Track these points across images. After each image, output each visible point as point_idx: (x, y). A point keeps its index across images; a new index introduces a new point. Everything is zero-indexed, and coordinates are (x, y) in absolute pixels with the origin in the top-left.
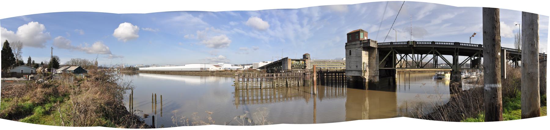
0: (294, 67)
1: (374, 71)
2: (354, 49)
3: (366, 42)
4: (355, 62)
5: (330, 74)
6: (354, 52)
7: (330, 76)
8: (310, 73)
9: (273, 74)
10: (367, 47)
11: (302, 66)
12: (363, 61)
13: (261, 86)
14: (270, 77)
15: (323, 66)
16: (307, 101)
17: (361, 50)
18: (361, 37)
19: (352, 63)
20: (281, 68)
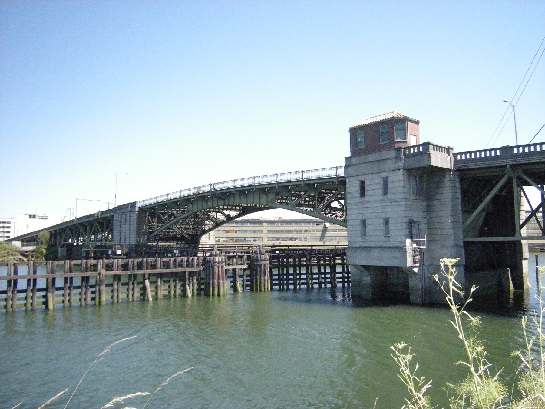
2: (374, 175)
3: (415, 154)
6: (377, 187)
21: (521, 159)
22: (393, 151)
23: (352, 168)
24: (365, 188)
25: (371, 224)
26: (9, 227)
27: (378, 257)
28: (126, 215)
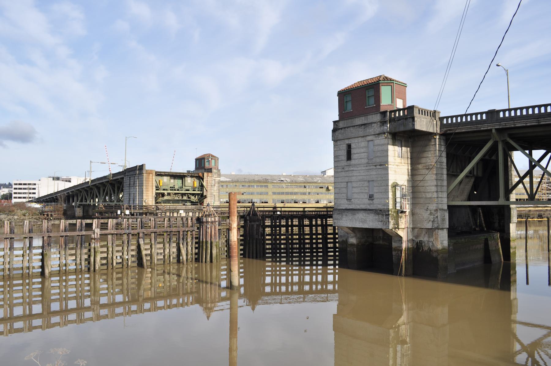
0: (166, 198)
2: (360, 139)
3: (400, 118)
4: (366, 184)
5: (283, 222)
6: (362, 150)
7: (283, 229)
8: (217, 219)
9: (89, 221)
10: (404, 132)
11: (193, 194)
12: (392, 178)
13: (42, 267)
14: (77, 233)
15: (261, 194)
16: (208, 310)
17: (386, 141)
18: (385, 100)
19: (354, 185)
20: (119, 200)
21: (506, 123)
22: (379, 115)
23: (340, 131)
24: (352, 151)
26: (34, 189)
27: (362, 219)
28: (130, 177)
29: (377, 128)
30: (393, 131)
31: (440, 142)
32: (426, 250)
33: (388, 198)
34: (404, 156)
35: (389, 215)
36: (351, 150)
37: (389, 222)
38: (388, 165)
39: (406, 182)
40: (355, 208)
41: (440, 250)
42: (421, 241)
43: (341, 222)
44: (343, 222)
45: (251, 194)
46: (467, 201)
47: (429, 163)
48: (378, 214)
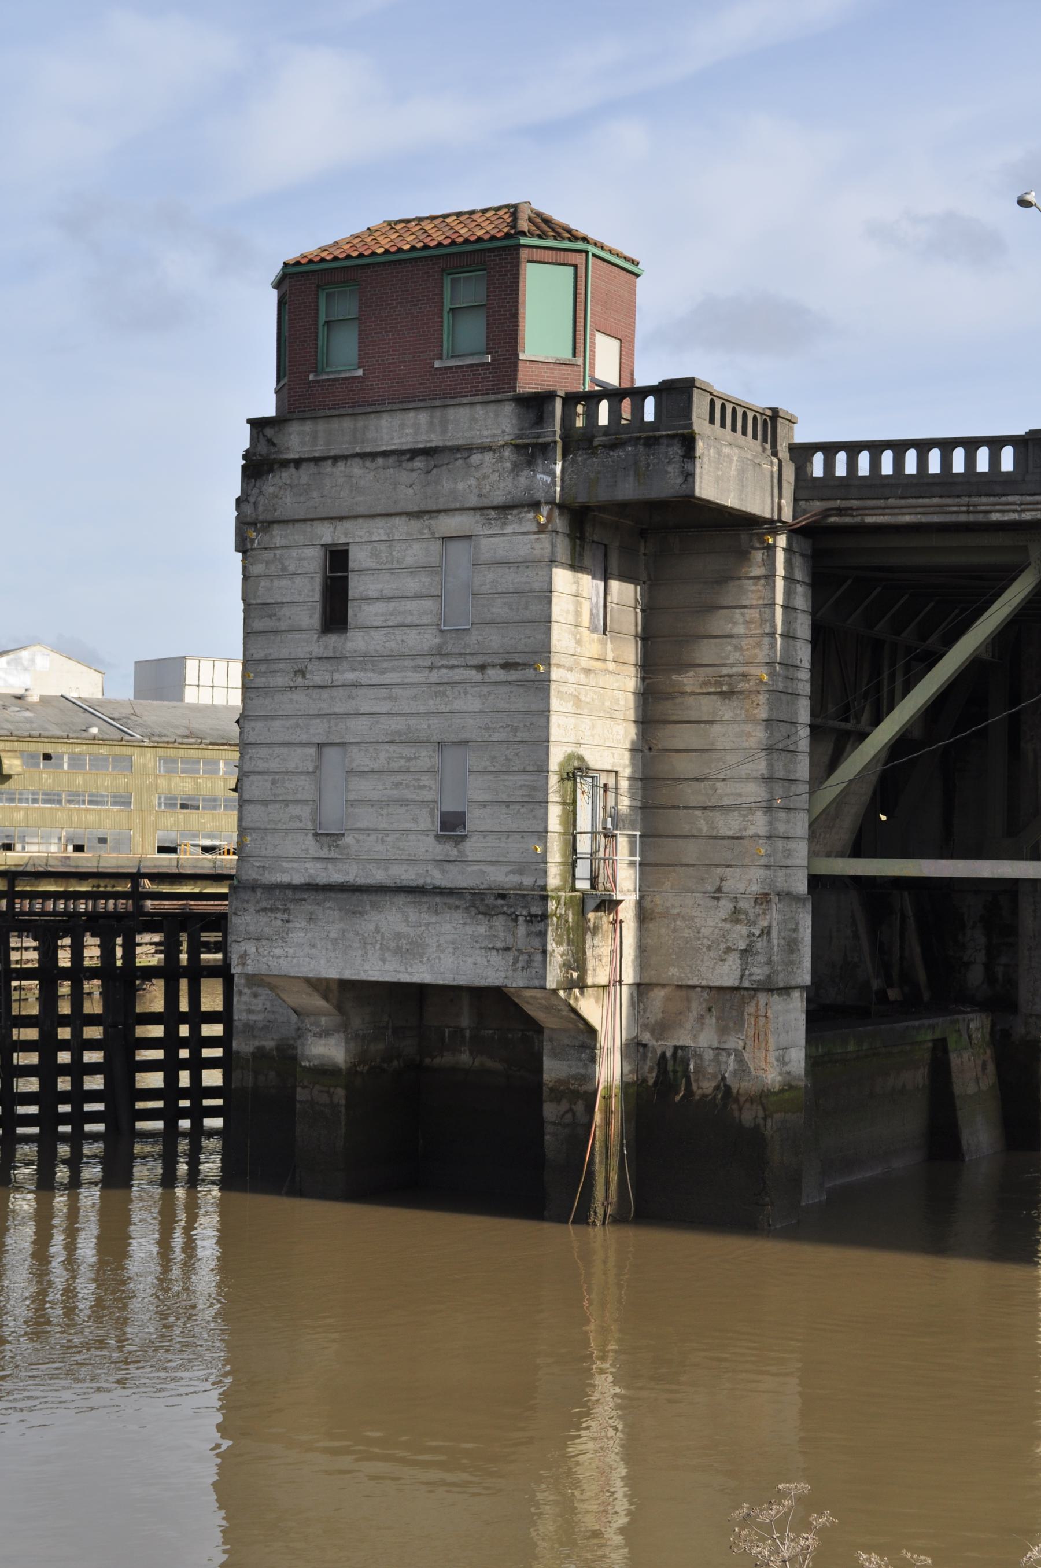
1: (736, 916)
2: (402, 527)
4: (426, 758)
6: (413, 584)
10: (623, 507)
17: (542, 545)
19: (360, 759)
22: (509, 408)
23: (286, 475)
25: (373, 772)
27: (399, 936)
29: (495, 477)
30: (580, 500)
31: (789, 564)
32: (704, 1096)
33: (542, 834)
34: (616, 627)
35: (544, 917)
36: (347, 578)
37: (544, 952)
38: (548, 665)
39: (627, 755)
40: (361, 881)
41: (776, 1094)
42: (683, 1048)
43: (278, 952)
44: (291, 951)
45: (184, 806)
46: (849, 857)
47: (732, 665)
48: (489, 913)
